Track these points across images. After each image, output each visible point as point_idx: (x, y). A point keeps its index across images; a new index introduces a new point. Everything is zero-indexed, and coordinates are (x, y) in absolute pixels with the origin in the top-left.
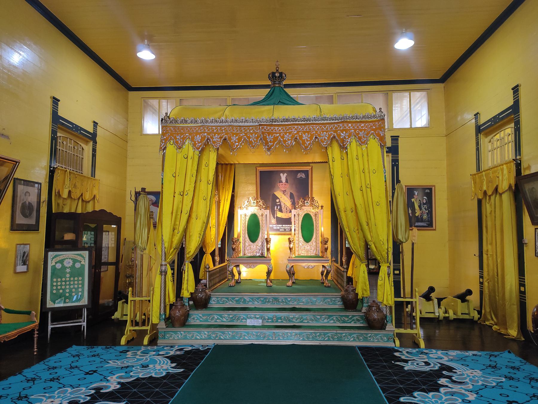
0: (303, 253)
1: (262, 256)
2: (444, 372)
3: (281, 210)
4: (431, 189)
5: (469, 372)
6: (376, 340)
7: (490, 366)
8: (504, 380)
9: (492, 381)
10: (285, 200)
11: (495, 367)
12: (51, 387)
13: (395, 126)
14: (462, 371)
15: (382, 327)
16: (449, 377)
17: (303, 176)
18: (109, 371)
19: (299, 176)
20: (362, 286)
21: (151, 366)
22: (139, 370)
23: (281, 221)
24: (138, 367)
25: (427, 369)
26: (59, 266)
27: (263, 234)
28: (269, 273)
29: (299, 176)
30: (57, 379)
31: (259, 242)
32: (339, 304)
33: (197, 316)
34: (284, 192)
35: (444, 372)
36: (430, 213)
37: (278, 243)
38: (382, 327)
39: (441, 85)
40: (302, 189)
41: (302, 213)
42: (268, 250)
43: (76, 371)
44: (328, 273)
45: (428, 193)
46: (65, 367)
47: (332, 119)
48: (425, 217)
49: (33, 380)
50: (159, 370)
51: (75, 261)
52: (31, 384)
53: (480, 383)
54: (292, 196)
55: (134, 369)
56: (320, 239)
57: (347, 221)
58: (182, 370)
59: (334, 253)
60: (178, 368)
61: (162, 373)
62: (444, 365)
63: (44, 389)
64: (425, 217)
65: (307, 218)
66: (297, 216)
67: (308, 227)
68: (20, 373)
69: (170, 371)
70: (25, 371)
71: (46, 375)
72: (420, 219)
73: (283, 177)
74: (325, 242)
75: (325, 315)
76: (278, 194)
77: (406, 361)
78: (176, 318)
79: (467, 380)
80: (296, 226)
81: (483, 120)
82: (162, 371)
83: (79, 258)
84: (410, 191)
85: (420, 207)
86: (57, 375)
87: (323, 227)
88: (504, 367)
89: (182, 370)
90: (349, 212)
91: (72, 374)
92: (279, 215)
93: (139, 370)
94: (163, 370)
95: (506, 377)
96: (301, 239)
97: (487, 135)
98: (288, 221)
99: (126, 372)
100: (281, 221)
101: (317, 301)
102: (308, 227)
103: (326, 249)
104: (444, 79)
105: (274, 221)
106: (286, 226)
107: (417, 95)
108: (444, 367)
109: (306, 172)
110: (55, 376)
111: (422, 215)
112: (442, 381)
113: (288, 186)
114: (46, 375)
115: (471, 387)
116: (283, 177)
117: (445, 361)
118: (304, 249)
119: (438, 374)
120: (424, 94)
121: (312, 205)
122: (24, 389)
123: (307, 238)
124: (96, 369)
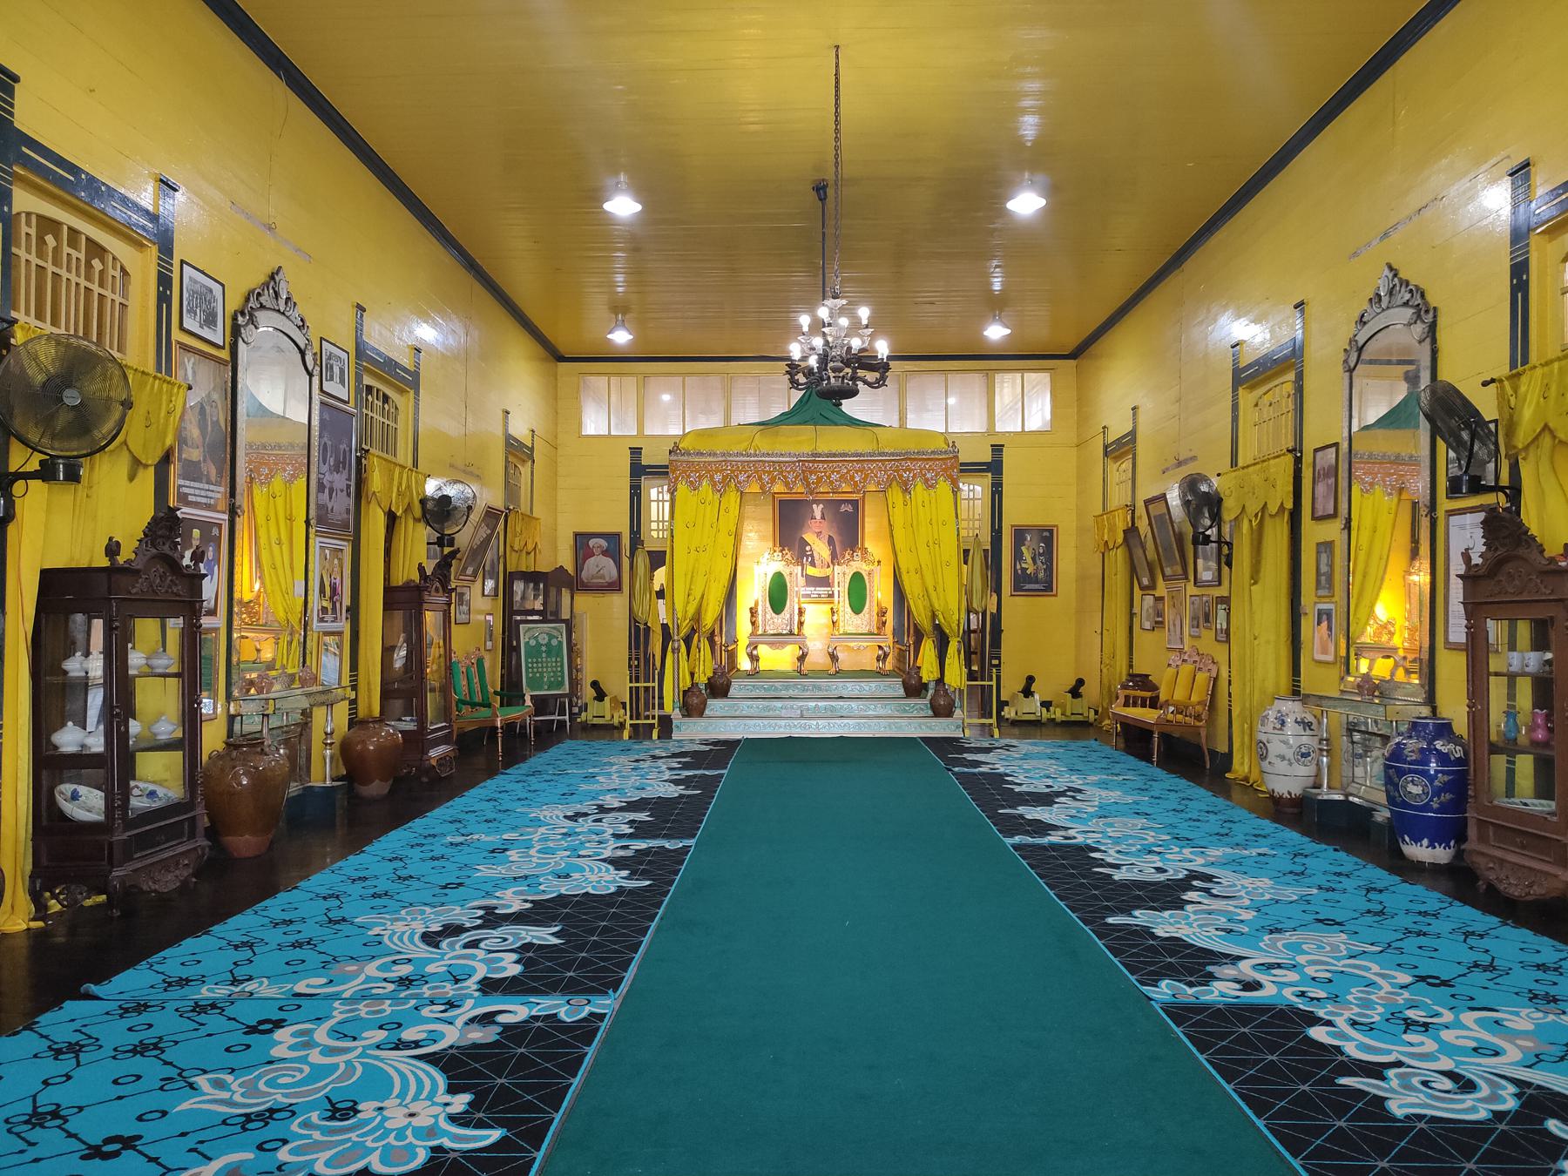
0: (851, 629)
1: (791, 633)
2: (1195, 883)
3: (813, 564)
4: (1051, 531)
5: (1247, 882)
6: (941, 728)
7: (1369, 912)
8: (1315, 891)
9: (1291, 893)
10: (821, 549)
11: (1491, 967)
12: (139, 1077)
13: (998, 429)
14: (1228, 879)
15: (949, 714)
16: (1207, 891)
17: (849, 508)
18: (190, 1141)
19: (843, 508)
20: (928, 672)
21: (367, 1108)
22: (317, 1135)
23: (812, 581)
24: (314, 1117)
25: (1161, 877)
26: (533, 643)
27: (792, 604)
28: (802, 659)
29: (843, 508)
30: (156, 1047)
31: (786, 614)
32: (902, 692)
33: (715, 706)
34: (819, 534)
35: (1195, 883)
36: (1049, 570)
37: (816, 618)
38: (949, 714)
39: (1072, 363)
40: (848, 535)
41: (850, 571)
42: (801, 624)
43: (213, 1021)
44: (886, 655)
45: (1047, 536)
46: (267, 948)
47: (892, 454)
48: (1041, 575)
49: (75, 1049)
50: (400, 1134)
51: (551, 637)
52: (67, 1063)
53: (1267, 896)
54: (831, 541)
55: (295, 1126)
56: (876, 609)
57: (911, 586)
58: (495, 1135)
59: (898, 632)
60: (481, 1125)
61: (410, 1151)
62: (1529, 1085)
63: (115, 1082)
64: (1041, 575)
65: (857, 580)
66: (841, 575)
67: (858, 592)
68: (29, 1028)
69: (447, 1143)
70: (45, 1019)
71: (117, 1034)
72: (1033, 579)
73: (817, 510)
74: (882, 613)
75: (879, 704)
76: (809, 537)
77: (1117, 867)
78: (692, 705)
79: (1242, 893)
80: (841, 589)
81: (1111, 438)
82: (411, 1139)
83: (555, 633)
84: (1020, 534)
85: (1034, 559)
86: (152, 1033)
87: (881, 592)
88: (1350, 890)
89: (495, 1135)
90: (912, 573)
91: (203, 1031)
92: (811, 571)
93: (317, 1135)
94: (418, 1132)
95: (1320, 888)
96: (849, 610)
97: (1116, 459)
98: (825, 582)
99: (260, 1147)
100: (812, 581)
101: (870, 687)
102: (858, 592)
103: (884, 623)
104: (1073, 355)
105: (802, 581)
106: (823, 590)
107: (1031, 377)
108: (1193, 875)
109: (855, 503)
110: (149, 1036)
111: (1036, 574)
112: (1190, 895)
113: (825, 524)
114: (117, 1034)
115: (1248, 903)
116: (817, 510)
117: (1198, 864)
118: (852, 623)
119: (1185, 884)
120: (1044, 377)
121: (864, 559)
122: (46, 1083)
123: (857, 608)
124: (248, 1039)
